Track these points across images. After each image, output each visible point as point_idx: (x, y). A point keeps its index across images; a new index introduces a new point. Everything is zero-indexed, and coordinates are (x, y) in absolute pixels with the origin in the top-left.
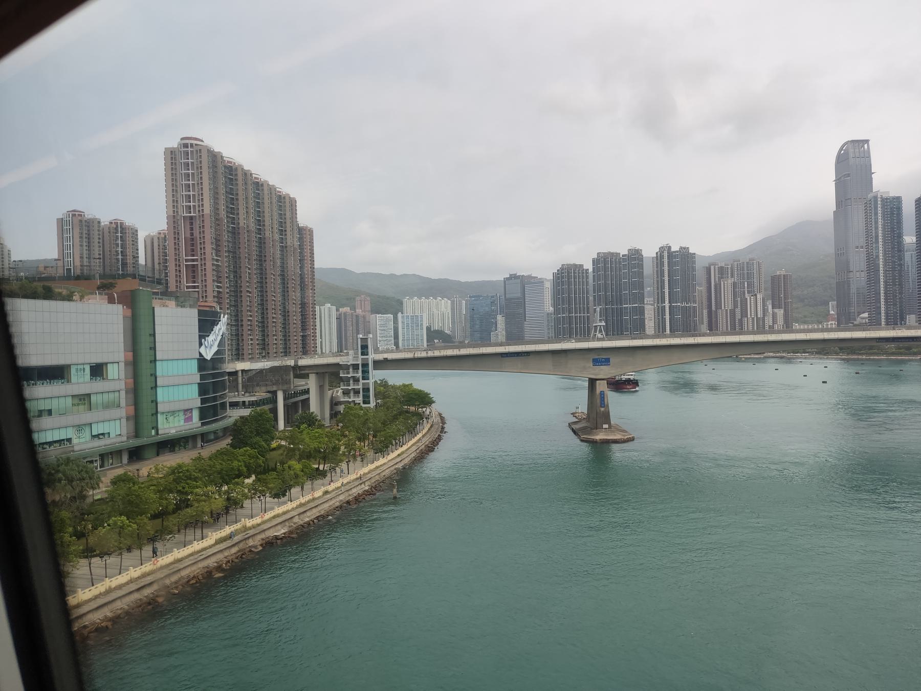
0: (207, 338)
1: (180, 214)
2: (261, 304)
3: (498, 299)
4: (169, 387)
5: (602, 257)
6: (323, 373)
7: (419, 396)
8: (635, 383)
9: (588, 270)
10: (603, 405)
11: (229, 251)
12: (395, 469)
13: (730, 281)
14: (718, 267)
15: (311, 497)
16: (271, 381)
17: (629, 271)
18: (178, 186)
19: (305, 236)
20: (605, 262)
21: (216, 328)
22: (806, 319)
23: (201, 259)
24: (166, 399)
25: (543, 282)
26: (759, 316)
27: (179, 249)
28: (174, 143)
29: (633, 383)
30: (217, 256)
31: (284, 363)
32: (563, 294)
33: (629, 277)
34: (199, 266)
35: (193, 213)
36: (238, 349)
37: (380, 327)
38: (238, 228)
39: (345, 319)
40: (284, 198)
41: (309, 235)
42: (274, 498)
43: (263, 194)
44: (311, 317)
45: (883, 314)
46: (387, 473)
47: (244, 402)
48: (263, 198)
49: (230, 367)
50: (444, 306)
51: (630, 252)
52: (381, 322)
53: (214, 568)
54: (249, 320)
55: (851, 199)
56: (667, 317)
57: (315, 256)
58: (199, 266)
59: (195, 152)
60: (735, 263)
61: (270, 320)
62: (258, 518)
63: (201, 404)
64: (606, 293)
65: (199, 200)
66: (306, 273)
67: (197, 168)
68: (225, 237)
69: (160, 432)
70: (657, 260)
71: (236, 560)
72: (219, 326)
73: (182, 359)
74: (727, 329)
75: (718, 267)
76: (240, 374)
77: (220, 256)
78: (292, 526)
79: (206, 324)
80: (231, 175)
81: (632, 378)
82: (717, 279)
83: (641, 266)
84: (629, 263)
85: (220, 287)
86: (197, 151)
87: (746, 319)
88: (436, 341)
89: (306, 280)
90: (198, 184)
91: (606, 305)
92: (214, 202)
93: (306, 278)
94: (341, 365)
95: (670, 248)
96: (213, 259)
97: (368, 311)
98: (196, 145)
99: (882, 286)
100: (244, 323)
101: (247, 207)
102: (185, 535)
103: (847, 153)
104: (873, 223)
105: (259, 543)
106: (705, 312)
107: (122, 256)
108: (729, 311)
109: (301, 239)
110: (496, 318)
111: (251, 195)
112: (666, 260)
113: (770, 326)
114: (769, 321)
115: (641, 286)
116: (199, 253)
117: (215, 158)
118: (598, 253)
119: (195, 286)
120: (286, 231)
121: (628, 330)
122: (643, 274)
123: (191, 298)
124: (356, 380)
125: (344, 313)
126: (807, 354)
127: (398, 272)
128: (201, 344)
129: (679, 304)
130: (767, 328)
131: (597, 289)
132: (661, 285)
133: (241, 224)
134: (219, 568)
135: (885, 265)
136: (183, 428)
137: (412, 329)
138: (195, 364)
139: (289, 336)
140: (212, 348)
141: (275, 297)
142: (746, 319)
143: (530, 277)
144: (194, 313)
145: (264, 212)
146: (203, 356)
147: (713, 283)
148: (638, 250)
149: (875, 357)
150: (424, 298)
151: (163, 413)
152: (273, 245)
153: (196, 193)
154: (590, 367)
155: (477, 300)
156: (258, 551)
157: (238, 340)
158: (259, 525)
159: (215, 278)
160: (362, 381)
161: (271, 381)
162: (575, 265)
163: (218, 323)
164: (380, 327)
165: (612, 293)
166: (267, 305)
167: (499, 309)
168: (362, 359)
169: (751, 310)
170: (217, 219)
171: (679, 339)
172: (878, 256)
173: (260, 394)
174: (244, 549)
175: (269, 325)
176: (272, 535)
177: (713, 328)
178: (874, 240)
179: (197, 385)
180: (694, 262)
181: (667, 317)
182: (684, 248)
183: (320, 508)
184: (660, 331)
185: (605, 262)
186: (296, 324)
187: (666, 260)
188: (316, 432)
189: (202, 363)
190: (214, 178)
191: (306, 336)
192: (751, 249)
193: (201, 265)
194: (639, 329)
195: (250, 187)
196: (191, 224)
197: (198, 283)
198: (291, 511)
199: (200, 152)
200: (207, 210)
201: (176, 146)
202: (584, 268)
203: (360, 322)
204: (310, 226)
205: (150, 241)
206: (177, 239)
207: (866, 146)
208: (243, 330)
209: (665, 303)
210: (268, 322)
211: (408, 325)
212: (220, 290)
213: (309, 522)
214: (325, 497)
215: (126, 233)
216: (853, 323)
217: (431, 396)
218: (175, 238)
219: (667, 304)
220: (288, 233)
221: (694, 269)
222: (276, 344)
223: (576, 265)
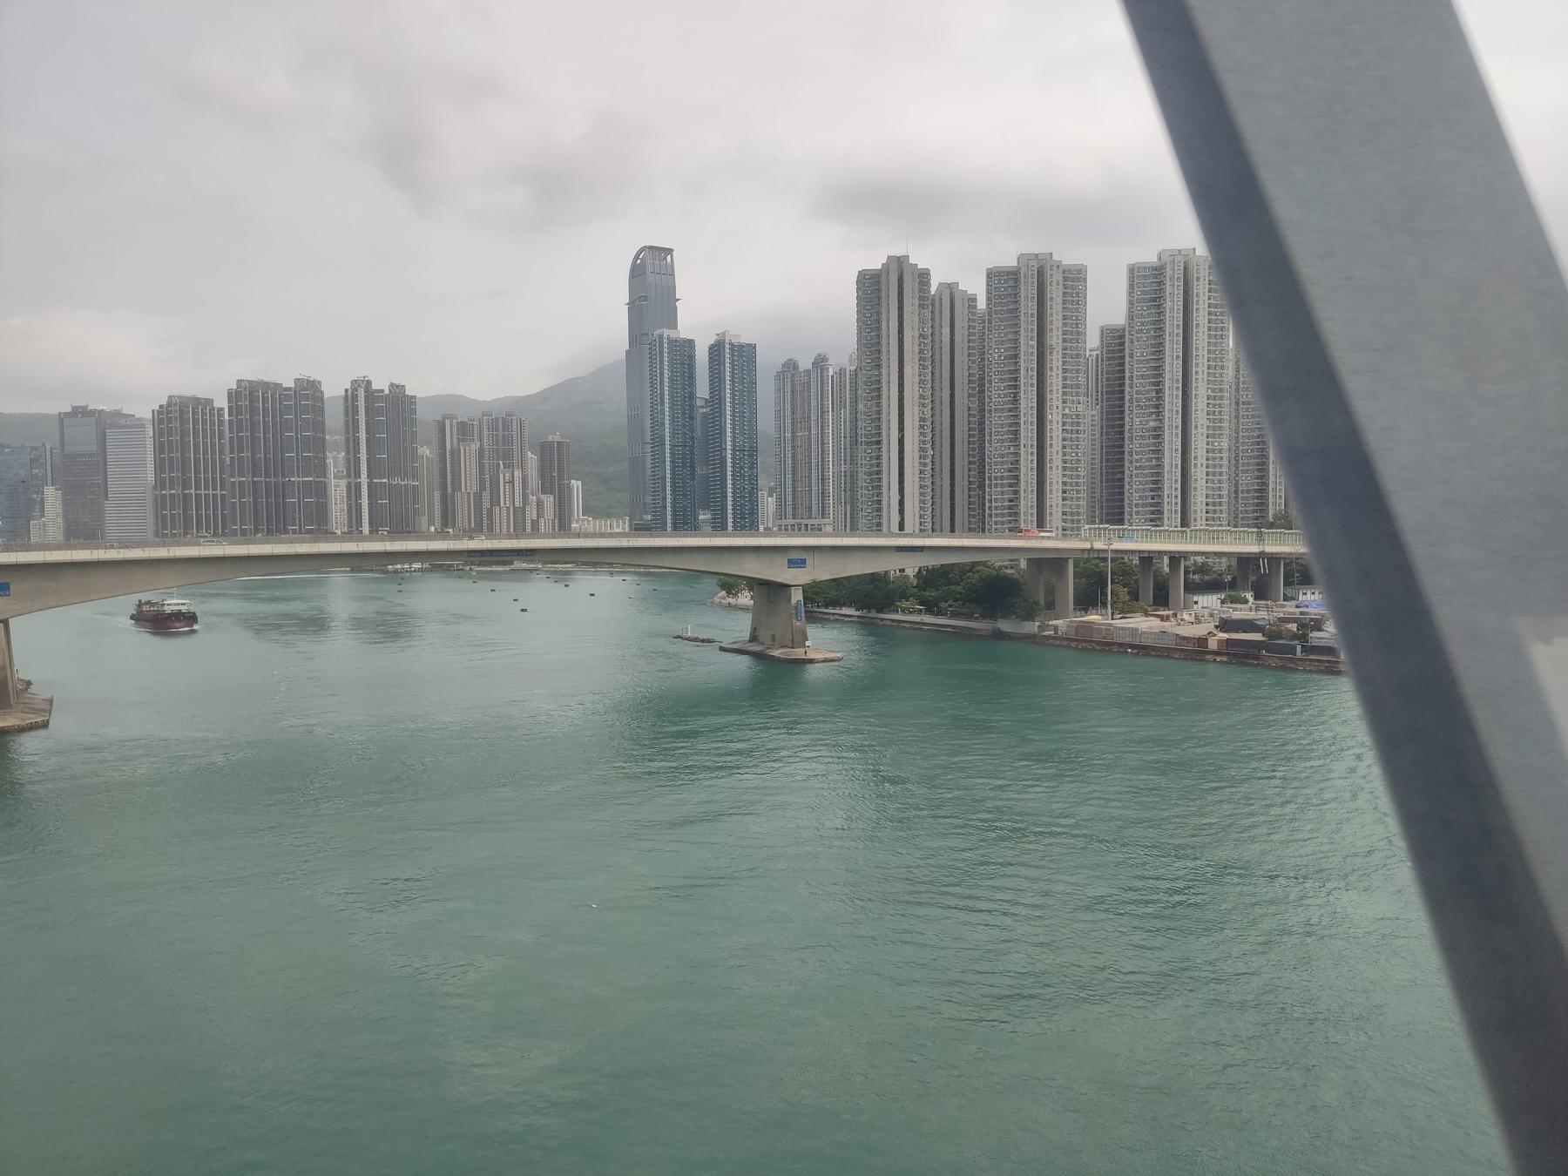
3: (48, 453)
8: (191, 618)
13: (475, 446)
14: (458, 423)
17: (296, 417)
22: (610, 511)
26: (517, 504)
32: (171, 451)
51: (299, 384)
55: (647, 334)
56: (365, 502)
60: (485, 418)
64: (253, 455)
70: (347, 402)
75: (458, 423)
81: (184, 609)
82: (455, 442)
84: (296, 404)
91: (254, 476)
95: (369, 383)
103: (643, 263)
104: (658, 371)
106: (437, 495)
108: (472, 495)
110: (43, 493)
112: (361, 404)
114: (531, 513)
115: (320, 446)
126: (570, 565)
132: (354, 446)
143: (118, 414)
147: (448, 448)
148: (314, 382)
162: (197, 401)
172: (663, 424)
180: (414, 412)
181: (365, 502)
182: (398, 386)
184: (353, 532)
185: (248, 396)
187: (361, 404)
192: (544, 396)
194: (318, 523)
202: (215, 406)
207: (669, 258)
209: (360, 478)
219: (364, 479)
221: (413, 422)
223: (198, 400)
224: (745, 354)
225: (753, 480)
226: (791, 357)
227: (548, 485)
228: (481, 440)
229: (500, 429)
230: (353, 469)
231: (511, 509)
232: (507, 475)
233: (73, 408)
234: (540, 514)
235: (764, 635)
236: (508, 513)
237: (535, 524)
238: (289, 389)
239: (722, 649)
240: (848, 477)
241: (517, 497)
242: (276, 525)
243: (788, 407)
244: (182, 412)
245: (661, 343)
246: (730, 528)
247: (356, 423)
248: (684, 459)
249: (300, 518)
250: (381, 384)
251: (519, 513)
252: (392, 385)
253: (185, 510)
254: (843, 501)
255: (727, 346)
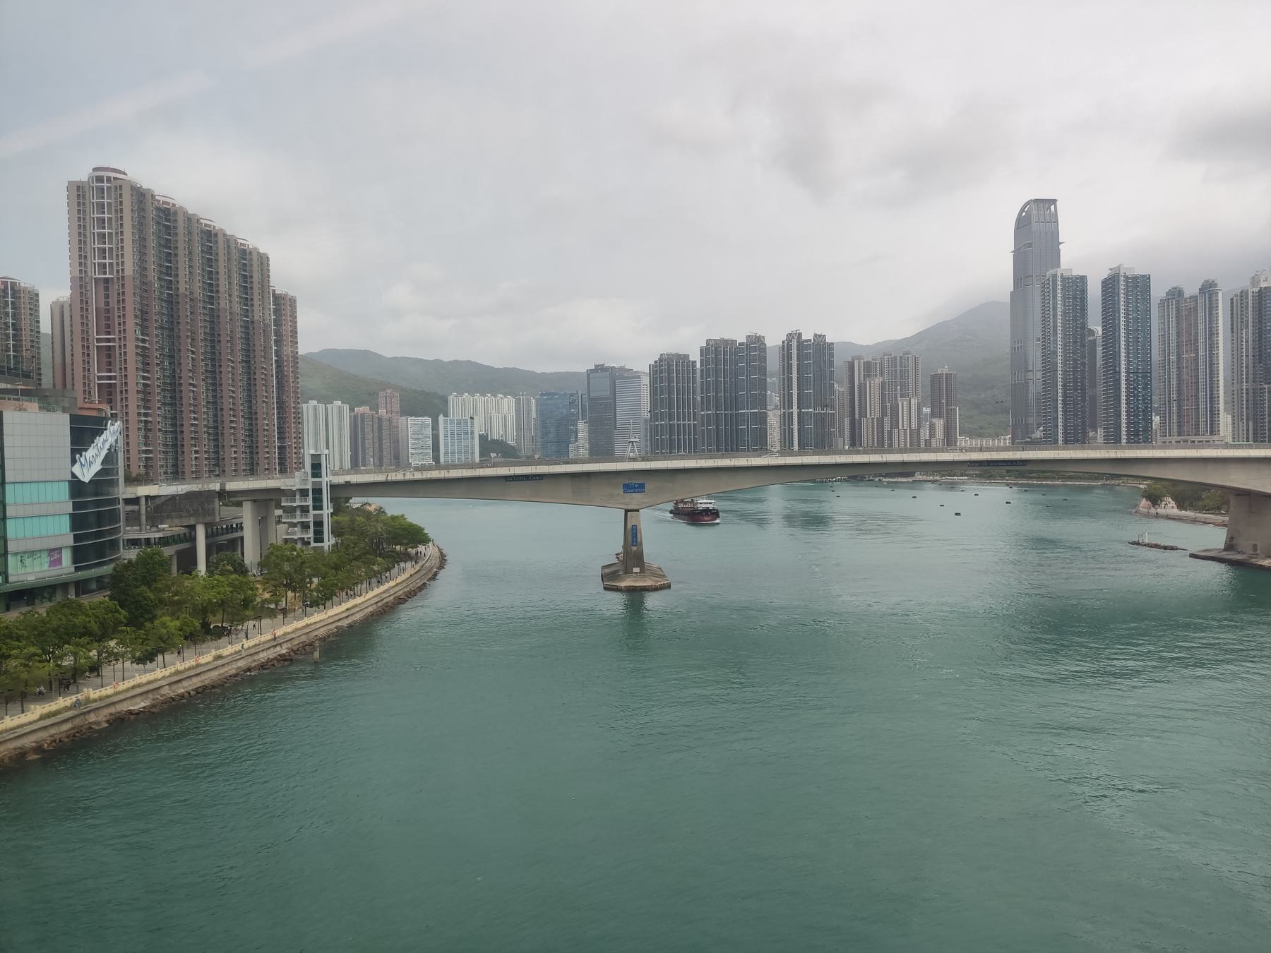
0: (83, 453)
1: (89, 274)
2: (213, 403)
3: (580, 398)
4: (34, 518)
5: (712, 346)
6: (266, 500)
7: (409, 532)
8: (715, 514)
9: (695, 362)
10: (635, 544)
11: (162, 328)
12: (337, 627)
13: (878, 380)
15: (194, 664)
16: (188, 511)
18: (88, 236)
19: (284, 306)
20: (716, 351)
21: (99, 440)
22: (981, 431)
23: (120, 339)
24: (21, 535)
25: (639, 377)
26: (913, 427)
27: (87, 324)
28: (83, 175)
29: (712, 514)
30: (142, 334)
31: (205, 487)
33: (747, 372)
34: (117, 348)
35: (109, 274)
36: (175, 466)
37: (413, 434)
38: (177, 296)
39: (363, 421)
40: (250, 253)
41: (290, 305)
42: (138, 664)
43: (217, 248)
44: (293, 420)
45: (1060, 428)
46: (322, 632)
47: (148, 540)
48: (217, 254)
49: (124, 491)
50: (507, 405)
52: (414, 428)
53: (32, 748)
54: (192, 425)
56: (795, 427)
57: (299, 335)
58: (117, 348)
59: (113, 189)
61: (227, 424)
62: (108, 688)
63: (75, 543)
64: (717, 394)
65: (117, 256)
66: (285, 359)
67: (116, 211)
68: (156, 307)
69: (11, 579)
70: (783, 351)
71: (66, 740)
72: (103, 437)
73: (52, 481)
74: (905, 445)
75: (864, 363)
76: (143, 501)
77: (148, 335)
78: (157, 699)
79: (83, 433)
80: (168, 220)
81: (711, 506)
83: (763, 359)
84: (747, 355)
85: (148, 378)
86: (116, 187)
87: (896, 431)
88: (493, 455)
89: (286, 369)
90: (117, 233)
92: (140, 259)
93: (286, 368)
94: (283, 490)
95: (800, 335)
96: (137, 339)
97: (397, 412)
98: (115, 178)
99: (1060, 391)
100: (184, 429)
101: (190, 266)
102: (6, 710)
105: (104, 719)
106: (847, 421)
107: (13, 330)
108: (875, 420)
109: (277, 311)
110: (577, 426)
111: (197, 249)
112: (794, 352)
113: (926, 440)
114: (924, 434)
115: (763, 386)
116: (117, 330)
117: (141, 196)
118: (707, 340)
119: (110, 376)
120: (252, 299)
121: (744, 443)
122: (765, 369)
123: (65, 399)
124: (305, 510)
125: (361, 414)
126: (966, 478)
127: (447, 357)
128: (74, 462)
129: (810, 410)
130: (922, 443)
131: (706, 387)
132: (788, 384)
133: (182, 290)
134: (38, 749)
135: (1064, 364)
136: (47, 574)
137: (459, 438)
138: (65, 488)
139: (257, 447)
140: (93, 466)
141: (233, 392)
142: (896, 431)
143: (622, 369)
144: (65, 419)
145: (218, 273)
146: (77, 477)
148: (759, 337)
149: (1048, 482)
150: (478, 395)
151: (16, 554)
152: (231, 319)
153: (113, 246)
154: (618, 495)
155: (551, 399)
156: (101, 729)
157: (176, 452)
158: (108, 697)
159: (140, 366)
160: (312, 512)
161: (188, 511)
163: (103, 433)
164: (413, 434)
165: (725, 393)
166: (222, 403)
167: (580, 412)
168: (313, 482)
169: (903, 419)
170: (144, 283)
171: (729, 460)
172: (1055, 353)
173: (167, 528)
174: (81, 726)
175: (225, 432)
176: (126, 710)
177: (855, 442)
178: (1051, 332)
179: (68, 516)
181: (795, 427)
182: (820, 336)
183: (203, 677)
184: (786, 449)
185: (716, 351)
186: (267, 430)
187: (794, 352)
188: (215, 580)
189: (76, 487)
190: (140, 225)
191: (285, 447)
192: (920, 337)
193: (120, 347)
195: (196, 238)
196: (107, 289)
197: (116, 372)
198: (160, 680)
199: (121, 189)
200: (129, 269)
201: (85, 179)
203: (384, 428)
204: (291, 293)
205: (59, 310)
206: (85, 309)
207: (1053, 207)
208: (183, 438)
210: (223, 428)
211: (452, 433)
212: (148, 382)
213: (183, 693)
214: (215, 663)
215: (20, 297)
216: (1030, 438)
217: (426, 531)
218: (82, 308)
219: (795, 410)
220: (256, 303)
221: (831, 363)
222: (235, 458)
224: (1140, 284)
225: (1147, 400)
226: (1175, 286)
227: (937, 410)
228: (882, 374)
229: (898, 365)
230: (787, 403)
231: (908, 431)
232: (905, 403)
233: (596, 366)
234: (932, 435)
235: (1244, 543)
236: (905, 435)
237: (928, 443)
238: (742, 344)
239: (1193, 556)
240: (1251, 394)
241: (913, 419)
242: (732, 445)
243: (1173, 332)
244: (669, 365)
245: (1055, 282)
246: (1124, 441)
247: (790, 366)
248: (1075, 382)
249: (748, 440)
250: (808, 335)
251: (915, 434)
252: (816, 335)
253: (670, 436)
254: (1245, 417)
255: (1122, 278)
